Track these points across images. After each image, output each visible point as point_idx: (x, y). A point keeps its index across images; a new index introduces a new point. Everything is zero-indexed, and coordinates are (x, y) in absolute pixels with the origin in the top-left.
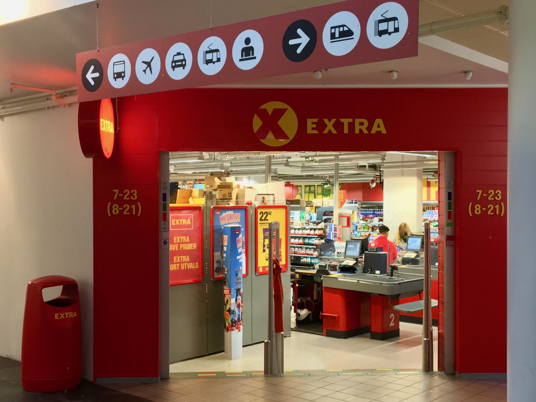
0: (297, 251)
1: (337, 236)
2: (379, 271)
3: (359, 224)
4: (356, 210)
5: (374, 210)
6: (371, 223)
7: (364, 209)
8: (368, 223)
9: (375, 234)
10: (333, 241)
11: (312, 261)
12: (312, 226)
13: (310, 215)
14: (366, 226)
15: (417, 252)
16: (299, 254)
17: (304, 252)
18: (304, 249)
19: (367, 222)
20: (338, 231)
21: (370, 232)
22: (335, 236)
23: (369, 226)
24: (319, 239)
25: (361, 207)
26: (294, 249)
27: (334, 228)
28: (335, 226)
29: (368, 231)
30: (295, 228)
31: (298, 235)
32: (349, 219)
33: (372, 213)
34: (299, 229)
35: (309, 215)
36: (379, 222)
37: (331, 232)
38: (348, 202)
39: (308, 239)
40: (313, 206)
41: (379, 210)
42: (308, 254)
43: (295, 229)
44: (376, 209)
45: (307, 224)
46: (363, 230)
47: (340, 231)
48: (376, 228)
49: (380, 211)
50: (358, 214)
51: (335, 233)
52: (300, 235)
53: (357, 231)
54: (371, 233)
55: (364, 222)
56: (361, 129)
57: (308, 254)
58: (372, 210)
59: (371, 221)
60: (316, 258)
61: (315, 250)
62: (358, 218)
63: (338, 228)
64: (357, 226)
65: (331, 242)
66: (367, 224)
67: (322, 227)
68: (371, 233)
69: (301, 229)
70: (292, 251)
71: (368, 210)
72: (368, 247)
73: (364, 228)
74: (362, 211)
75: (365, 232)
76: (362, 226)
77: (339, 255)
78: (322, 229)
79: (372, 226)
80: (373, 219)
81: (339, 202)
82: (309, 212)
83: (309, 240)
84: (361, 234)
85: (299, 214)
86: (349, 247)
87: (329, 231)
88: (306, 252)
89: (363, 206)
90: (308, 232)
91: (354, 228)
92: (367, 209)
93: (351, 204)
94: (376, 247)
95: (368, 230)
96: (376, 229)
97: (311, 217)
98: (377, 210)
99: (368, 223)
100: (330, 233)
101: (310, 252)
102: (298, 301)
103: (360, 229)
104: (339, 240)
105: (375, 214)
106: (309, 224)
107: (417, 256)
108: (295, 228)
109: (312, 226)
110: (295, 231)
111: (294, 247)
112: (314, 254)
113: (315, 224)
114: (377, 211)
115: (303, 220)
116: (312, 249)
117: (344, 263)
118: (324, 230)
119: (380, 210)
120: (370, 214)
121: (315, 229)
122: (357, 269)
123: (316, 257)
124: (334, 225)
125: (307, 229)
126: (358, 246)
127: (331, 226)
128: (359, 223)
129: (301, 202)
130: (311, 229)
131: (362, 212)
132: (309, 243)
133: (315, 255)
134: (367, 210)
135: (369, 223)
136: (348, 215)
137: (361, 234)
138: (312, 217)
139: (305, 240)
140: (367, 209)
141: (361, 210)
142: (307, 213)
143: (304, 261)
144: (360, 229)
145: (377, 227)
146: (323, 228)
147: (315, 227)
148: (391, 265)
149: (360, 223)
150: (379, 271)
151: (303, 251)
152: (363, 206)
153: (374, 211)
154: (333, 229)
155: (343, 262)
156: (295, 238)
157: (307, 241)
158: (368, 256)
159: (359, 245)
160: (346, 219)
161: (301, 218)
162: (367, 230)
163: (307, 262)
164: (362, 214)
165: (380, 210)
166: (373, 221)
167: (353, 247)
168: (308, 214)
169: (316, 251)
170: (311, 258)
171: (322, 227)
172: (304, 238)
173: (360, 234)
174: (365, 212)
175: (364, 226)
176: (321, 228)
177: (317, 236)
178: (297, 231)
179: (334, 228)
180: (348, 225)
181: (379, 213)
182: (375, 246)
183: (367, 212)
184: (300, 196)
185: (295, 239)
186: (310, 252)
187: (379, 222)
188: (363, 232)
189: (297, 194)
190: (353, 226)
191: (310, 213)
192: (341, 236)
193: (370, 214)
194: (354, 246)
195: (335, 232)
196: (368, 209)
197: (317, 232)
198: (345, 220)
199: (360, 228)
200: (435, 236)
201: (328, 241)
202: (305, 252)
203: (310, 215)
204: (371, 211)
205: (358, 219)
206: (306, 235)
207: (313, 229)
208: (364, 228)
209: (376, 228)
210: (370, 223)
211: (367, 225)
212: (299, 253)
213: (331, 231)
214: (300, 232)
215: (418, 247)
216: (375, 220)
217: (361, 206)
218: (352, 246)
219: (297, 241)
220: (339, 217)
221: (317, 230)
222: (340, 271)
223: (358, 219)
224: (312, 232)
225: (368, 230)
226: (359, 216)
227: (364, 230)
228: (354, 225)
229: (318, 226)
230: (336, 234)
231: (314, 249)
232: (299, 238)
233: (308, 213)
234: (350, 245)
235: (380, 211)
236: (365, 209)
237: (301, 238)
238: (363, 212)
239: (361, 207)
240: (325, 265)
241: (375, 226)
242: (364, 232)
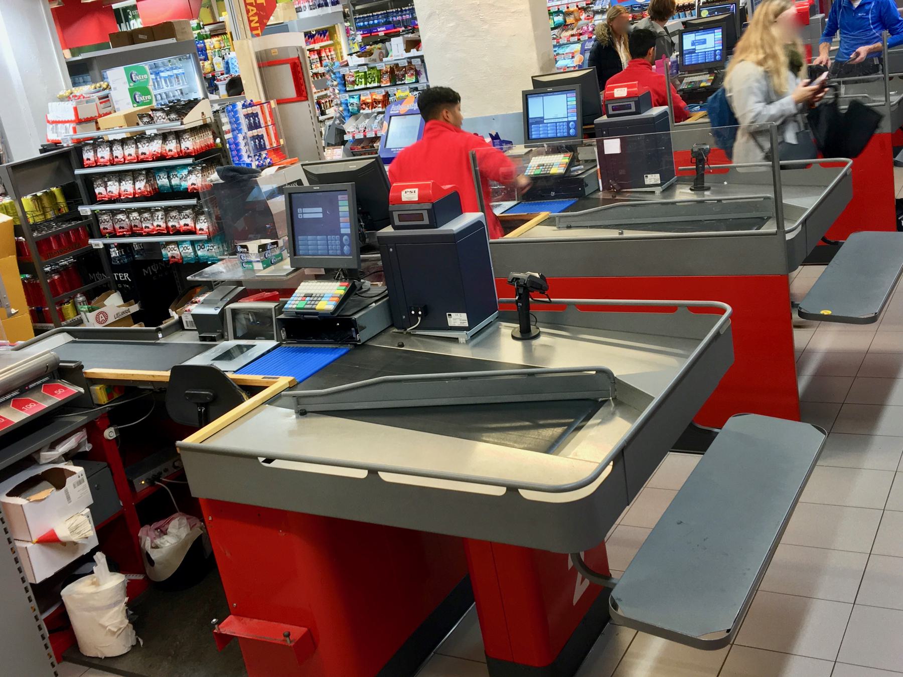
0: (137, 223)
1: (268, 147)
2: (464, 316)
3: (347, 69)
4: (341, 23)
5: (387, 13)
6: (384, 59)
7: (361, 16)
8: (375, 60)
9: (403, 91)
10: (254, 173)
11: (200, 253)
12: (164, 123)
13: (223, 59)
14: (372, 71)
15: (570, 149)
16: (149, 235)
17: (163, 225)
18: (160, 214)
19: (373, 57)
20: (267, 127)
21: (388, 89)
22: (260, 148)
23: (380, 70)
24: (203, 170)
25: (355, 12)
26: (128, 217)
27: (247, 116)
28: (249, 110)
29: (380, 87)
30: (111, 138)
31: (124, 163)
32: (297, 69)
33: (382, 21)
34: (123, 142)
35: (221, 59)
36: (407, 50)
37: (240, 137)
38: (314, 5)
39: (163, 175)
40: (226, 34)
41: (397, 12)
42: (178, 232)
43: (111, 144)
44: (391, 11)
45: (146, 120)
46: (363, 86)
47: (273, 124)
48: (402, 73)
49: (400, 13)
50: (347, 31)
51: (254, 138)
52: (131, 163)
53: (346, 91)
54: (391, 90)
55: (362, 60)
56: (405, 50)
57: (178, 232)
58: (381, 14)
59: (384, 51)
60: (209, 240)
61: (197, 212)
62: (351, 42)
63: (263, 113)
64: (344, 76)
65: (245, 177)
66: (372, 65)
67: (204, 120)
68: (391, 90)
69: (128, 138)
70: (124, 224)
71: (373, 16)
72: (391, 207)
73: (366, 78)
74: (359, 22)
75: (372, 91)
76: (360, 74)
77: (268, 254)
78: (205, 127)
79: (389, 67)
80: (387, 43)
81: (250, 8)
82: (219, 51)
83: (169, 177)
84: (363, 98)
85: (125, 78)
86: (306, 216)
87: (233, 130)
88: (170, 224)
89: (358, 8)
90: (155, 147)
91: (335, 83)
92: (368, 15)
93: (325, 8)
94: (428, 206)
95: (379, 81)
96: (404, 76)
97: (227, 63)
98: (393, 12)
99: (375, 60)
100: (235, 138)
101: (182, 222)
102: (138, 489)
103: (354, 83)
104: (275, 159)
105: (389, 23)
106: (152, 119)
107: (574, 161)
108: (108, 141)
109: (164, 123)
110: (111, 150)
111: (128, 212)
112: (198, 227)
113: (173, 116)
114: (395, 14)
115: (142, 99)
116: (188, 212)
117: (294, 303)
118: (214, 128)
119: (402, 11)
120: (379, 25)
121: (178, 135)
122: (359, 323)
123: (205, 237)
124: (244, 106)
125: (151, 139)
126: (341, 209)
127: (236, 113)
128: (347, 65)
129: (176, 27)
130: (165, 137)
131: (359, 24)
132: (171, 186)
133: (201, 229)
134: (370, 16)
135: (378, 60)
136: (293, 55)
137: (363, 98)
138: (229, 61)
139: (158, 178)
140: (368, 15)
141: (356, 19)
142: (215, 55)
143: (173, 257)
144: (354, 83)
145: (405, 67)
146: (208, 121)
147: (176, 126)
148: (517, 279)
149: (351, 64)
150: (464, 316)
151: (159, 222)
152: (358, 8)
153: (387, 15)
154: (244, 123)
155: (289, 292)
156: (120, 176)
157: (163, 181)
158: (395, 249)
159: (346, 203)
160: (287, 70)
161: (138, 93)
162: (376, 84)
163: (182, 258)
164: (359, 29)
165: (402, 11)
166: (389, 50)
167: (321, 216)
168: (217, 57)
169: (202, 218)
170: (193, 243)
171: (204, 120)
172: (150, 173)
173: (360, 99)
174: (366, 23)
175: (365, 72)
176: (201, 123)
177: (190, 161)
178: (118, 152)
179: (247, 116)
180: (302, 93)
181: (399, 18)
182: (422, 199)
183: (371, 22)
184: (208, 10)
185: (120, 182)
186: (182, 222)
187: (407, 50)
188: (365, 92)
189: (201, 7)
190: (333, 76)
191: (223, 52)
192: (282, 142)
193: (379, 25)
194: (324, 212)
195: (255, 132)
196: (371, 14)
197: (189, 144)
198: (285, 73)
199: (353, 79)
200: (558, 54)
201: (232, 174)
202: (166, 223)
203: (223, 59)
204: (380, 17)
205: (349, 44)
206: (153, 161)
207: (170, 133)
208: (366, 77)
209: (402, 73)
210: (381, 60)
211: (373, 68)
212: (147, 230)
213: (240, 131)
214: (130, 150)
215: (569, 129)
216: (394, 47)
217: (352, 9)
218: (311, 213)
219: (127, 187)
220: (259, 67)
221: (186, 136)
222: (284, 335)
223: (349, 44)
224: (172, 146)
225: (379, 81)
226: (351, 38)
227: (369, 85)
228: (334, 74)
229: (186, 120)
230: (260, 137)
231: (192, 207)
232: (134, 175)
233: (217, 54)
234: (306, 210)
235: (400, 13)
236: (365, 15)
237: (141, 174)
238: (362, 24)
239: (355, 12)
240: (217, 312)
241: (397, 65)
242: (368, 92)
